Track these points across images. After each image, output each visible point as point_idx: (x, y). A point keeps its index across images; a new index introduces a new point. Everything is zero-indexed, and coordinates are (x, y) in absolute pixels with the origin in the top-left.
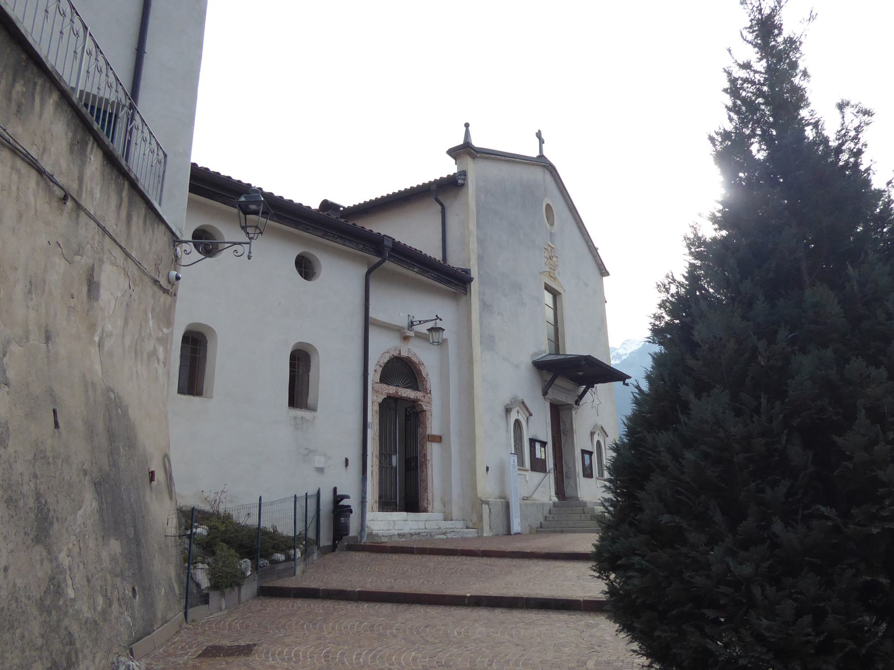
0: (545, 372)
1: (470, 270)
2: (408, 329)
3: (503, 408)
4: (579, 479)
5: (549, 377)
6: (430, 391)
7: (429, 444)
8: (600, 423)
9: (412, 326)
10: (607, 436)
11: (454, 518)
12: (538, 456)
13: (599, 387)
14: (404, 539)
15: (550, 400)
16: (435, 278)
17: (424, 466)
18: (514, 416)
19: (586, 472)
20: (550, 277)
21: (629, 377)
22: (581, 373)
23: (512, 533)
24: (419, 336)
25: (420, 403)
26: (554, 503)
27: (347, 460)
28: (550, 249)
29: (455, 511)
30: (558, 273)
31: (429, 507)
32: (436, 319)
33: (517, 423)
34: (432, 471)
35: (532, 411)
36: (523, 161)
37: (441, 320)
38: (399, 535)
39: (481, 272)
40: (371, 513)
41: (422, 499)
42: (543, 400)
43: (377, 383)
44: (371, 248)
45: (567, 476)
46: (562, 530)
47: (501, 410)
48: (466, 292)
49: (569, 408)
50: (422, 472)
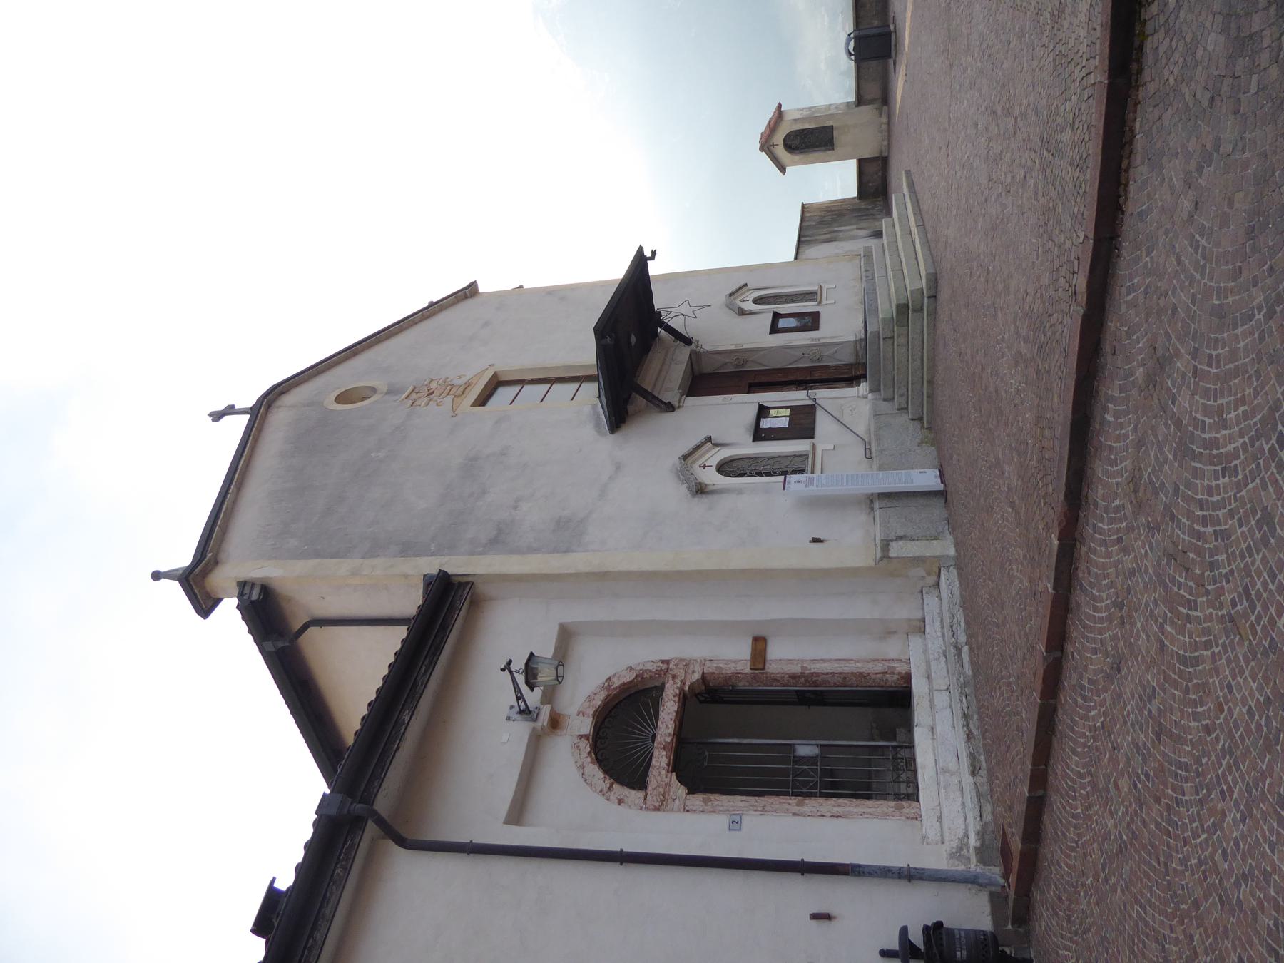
0: (630, 408)
1: (425, 576)
2: (536, 720)
3: (696, 499)
4: (823, 338)
5: (640, 401)
6: (663, 662)
7: (772, 668)
8: (722, 298)
9: (530, 712)
10: (746, 285)
11: (919, 615)
12: (784, 423)
13: (658, 303)
14: (982, 757)
15: (682, 396)
16: (431, 662)
17: (814, 679)
18: (711, 477)
19: (810, 325)
20: (465, 395)
21: (641, 250)
22: (633, 339)
23: (941, 487)
24: (549, 697)
25: (687, 688)
26: (871, 391)
27: (815, 917)
28: (414, 396)
29: (904, 612)
30: (460, 377)
31: (898, 670)
32: (511, 672)
33: (725, 468)
34: (824, 661)
35: (701, 437)
36: (245, 454)
37: (510, 662)
38: (973, 773)
39: (433, 548)
40: (924, 822)
41: (882, 683)
42: (681, 409)
43: (645, 799)
44: (345, 843)
45: (818, 360)
46: (928, 382)
47: (701, 504)
48: (467, 583)
49: (696, 358)
50: (826, 682)
